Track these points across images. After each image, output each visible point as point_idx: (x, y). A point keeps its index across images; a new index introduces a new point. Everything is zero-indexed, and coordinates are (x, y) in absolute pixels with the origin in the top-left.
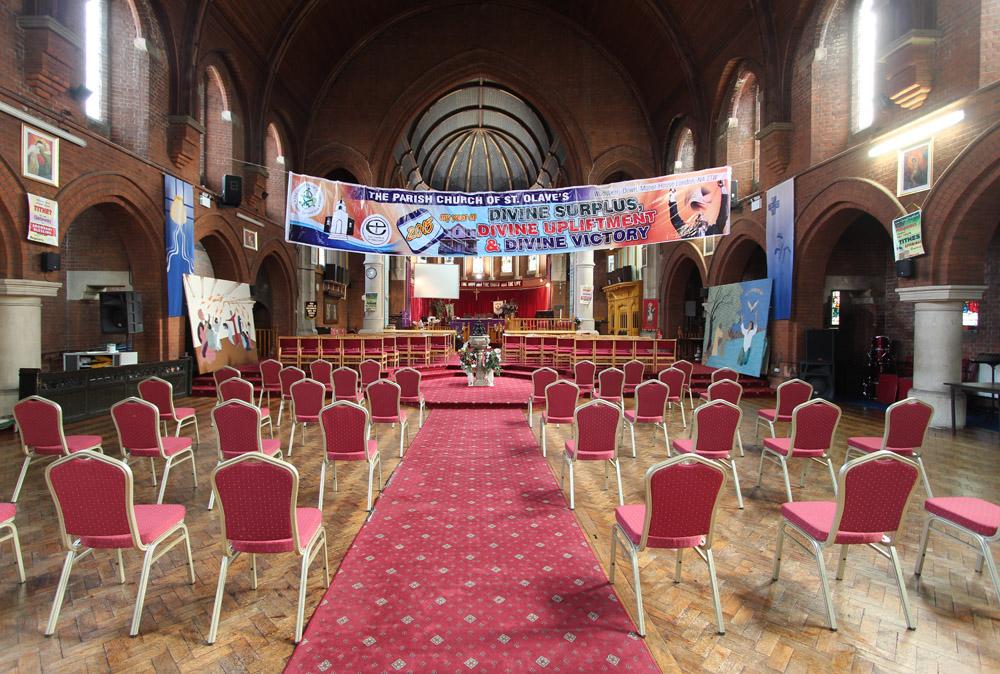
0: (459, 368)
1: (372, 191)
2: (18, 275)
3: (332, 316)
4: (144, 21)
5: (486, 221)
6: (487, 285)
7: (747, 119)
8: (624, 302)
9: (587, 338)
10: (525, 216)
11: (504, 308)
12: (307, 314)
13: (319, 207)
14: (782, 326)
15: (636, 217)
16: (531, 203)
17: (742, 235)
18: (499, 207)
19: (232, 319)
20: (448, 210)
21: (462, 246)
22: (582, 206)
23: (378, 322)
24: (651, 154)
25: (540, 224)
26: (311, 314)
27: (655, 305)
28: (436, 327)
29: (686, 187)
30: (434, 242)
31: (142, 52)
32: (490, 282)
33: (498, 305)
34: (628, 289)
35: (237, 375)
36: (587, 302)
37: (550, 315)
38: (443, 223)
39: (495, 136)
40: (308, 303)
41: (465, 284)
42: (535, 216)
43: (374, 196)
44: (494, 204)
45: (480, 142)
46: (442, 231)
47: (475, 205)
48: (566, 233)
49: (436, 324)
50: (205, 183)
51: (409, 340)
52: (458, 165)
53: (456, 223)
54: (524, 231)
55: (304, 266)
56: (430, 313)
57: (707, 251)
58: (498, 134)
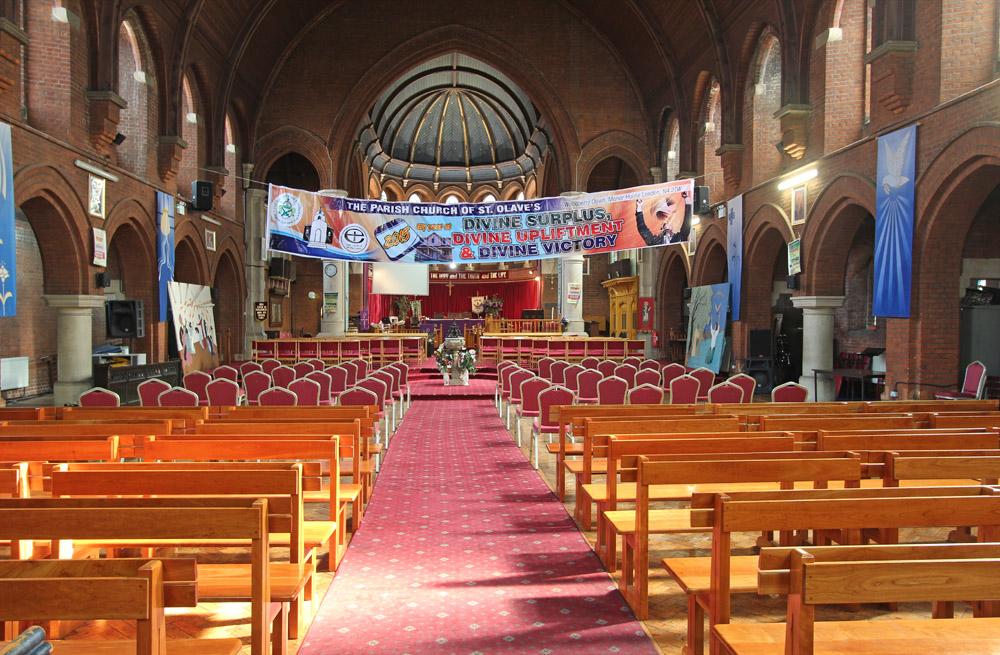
0: (437, 371)
1: (350, 202)
2: (86, 292)
3: (277, 319)
4: (143, 57)
5: (461, 230)
6: (463, 276)
7: (856, 34)
8: (624, 299)
9: (577, 339)
10: (498, 224)
11: (485, 306)
12: (256, 316)
13: (298, 217)
14: (737, 325)
15: (604, 225)
16: (504, 213)
17: (845, 198)
18: (473, 217)
19: (200, 324)
20: (424, 219)
21: (438, 253)
22: (552, 216)
23: (338, 327)
24: (645, 140)
25: (513, 233)
26: (261, 316)
27: (651, 305)
28: (400, 329)
29: (652, 198)
30: (410, 250)
31: (141, 84)
32: (467, 273)
33: (477, 301)
34: (627, 286)
35: (259, 368)
36: (575, 302)
37: (540, 314)
38: (420, 232)
39: (474, 97)
40: (257, 304)
41: (435, 276)
42: (507, 225)
43: (352, 206)
44: (469, 214)
45: (454, 102)
46: (418, 240)
47: (450, 215)
48: (538, 241)
49: (400, 326)
50: (182, 192)
51: (382, 344)
52: (427, 129)
53: (431, 232)
54: (497, 239)
55: (253, 262)
56: (391, 312)
57: (796, 219)
58: (477, 95)
